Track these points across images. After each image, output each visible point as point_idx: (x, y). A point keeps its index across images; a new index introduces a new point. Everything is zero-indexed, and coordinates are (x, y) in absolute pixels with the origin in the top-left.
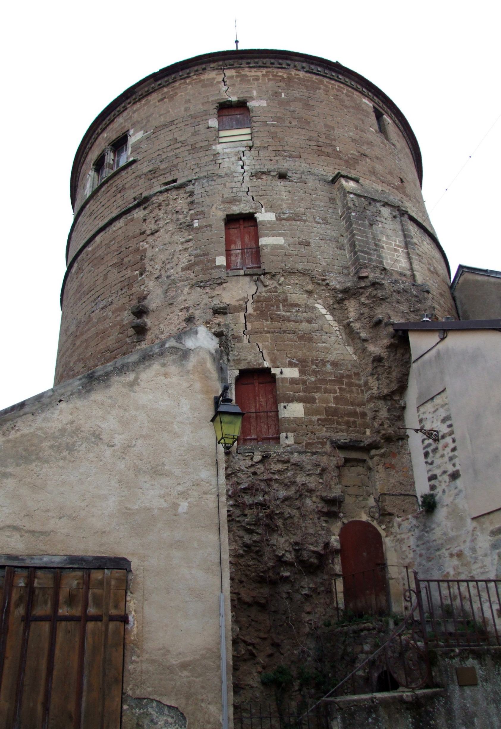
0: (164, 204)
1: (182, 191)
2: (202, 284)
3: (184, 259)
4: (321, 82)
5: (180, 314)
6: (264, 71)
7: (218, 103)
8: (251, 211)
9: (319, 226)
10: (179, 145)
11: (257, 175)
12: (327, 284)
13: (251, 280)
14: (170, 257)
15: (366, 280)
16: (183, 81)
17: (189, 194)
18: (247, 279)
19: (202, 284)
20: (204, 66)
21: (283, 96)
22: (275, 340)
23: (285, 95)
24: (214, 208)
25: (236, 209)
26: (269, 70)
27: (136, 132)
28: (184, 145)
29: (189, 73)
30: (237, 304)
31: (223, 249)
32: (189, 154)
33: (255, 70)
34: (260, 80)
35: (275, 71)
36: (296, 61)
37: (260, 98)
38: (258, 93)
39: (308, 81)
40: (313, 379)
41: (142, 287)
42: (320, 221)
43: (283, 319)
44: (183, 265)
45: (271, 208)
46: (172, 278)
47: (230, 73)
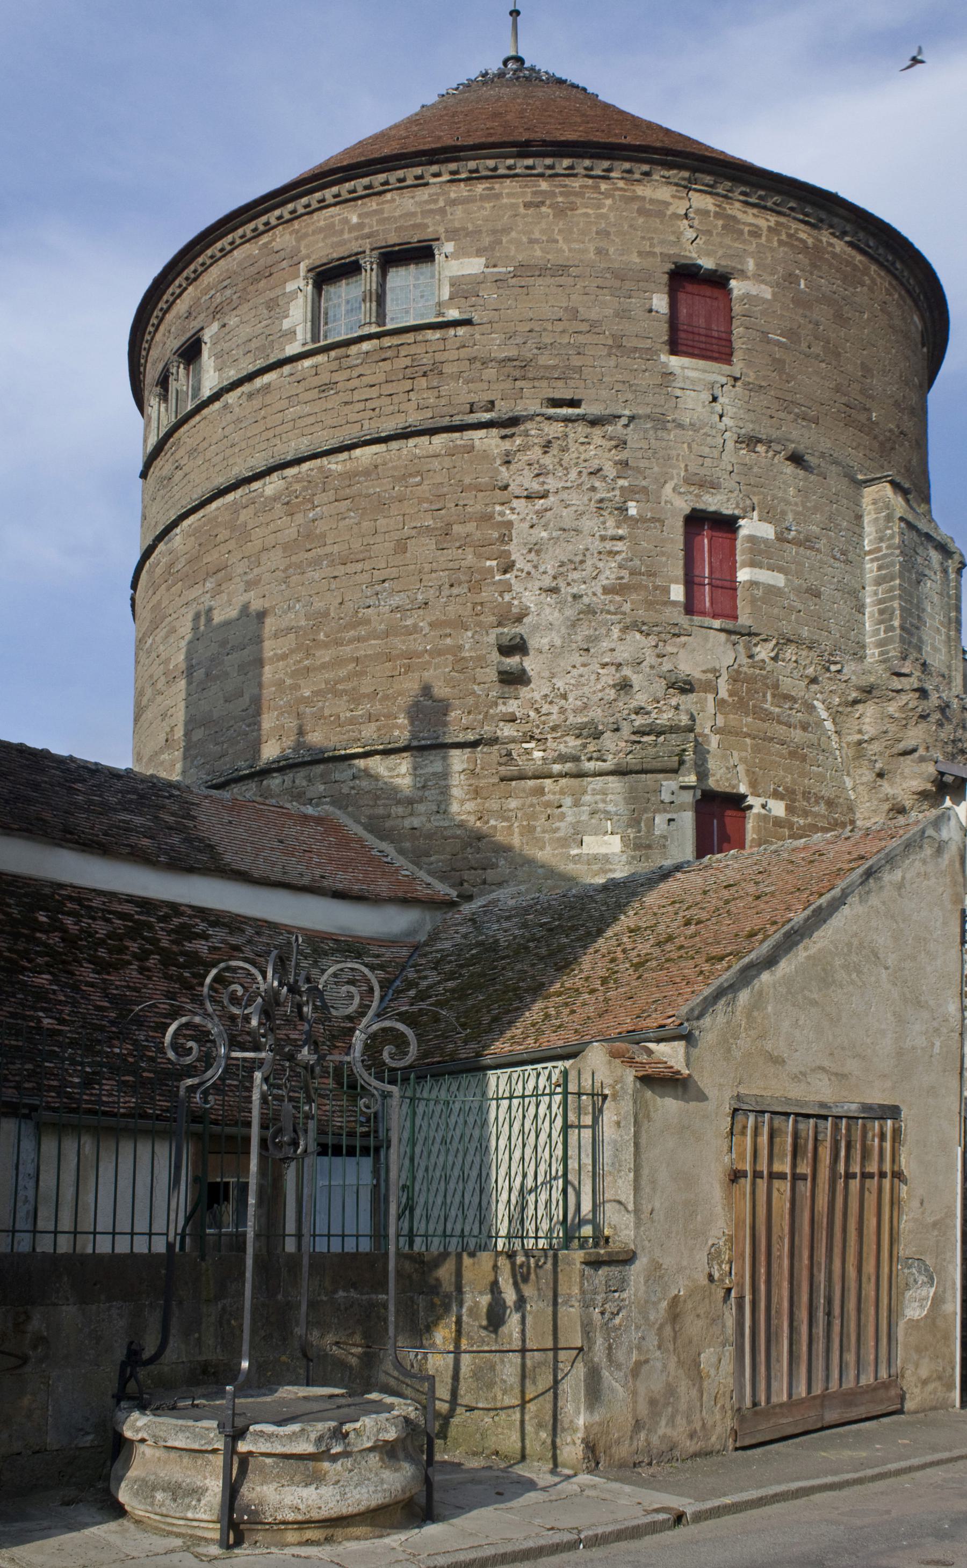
1: (597, 431)
2: (644, 628)
3: (610, 572)
4: (866, 272)
5: (600, 671)
6: (773, 219)
7: (675, 263)
8: (737, 512)
9: (837, 564)
10: (584, 327)
11: (751, 441)
13: (728, 640)
14: (578, 559)
16: (590, 182)
17: (613, 443)
18: (723, 636)
19: (644, 628)
20: (646, 168)
21: (802, 286)
22: (756, 750)
23: (806, 286)
24: (668, 488)
25: (713, 502)
26: (782, 220)
27: (460, 253)
28: (596, 330)
29: (609, 170)
30: (703, 677)
31: (680, 572)
32: (609, 355)
33: (755, 211)
34: (764, 238)
35: (794, 225)
36: (837, 215)
37: (758, 278)
38: (757, 265)
39: (848, 263)
40: (802, 822)
41: (507, 597)
42: (838, 555)
43: (768, 717)
44: (605, 582)
47: (701, 201)
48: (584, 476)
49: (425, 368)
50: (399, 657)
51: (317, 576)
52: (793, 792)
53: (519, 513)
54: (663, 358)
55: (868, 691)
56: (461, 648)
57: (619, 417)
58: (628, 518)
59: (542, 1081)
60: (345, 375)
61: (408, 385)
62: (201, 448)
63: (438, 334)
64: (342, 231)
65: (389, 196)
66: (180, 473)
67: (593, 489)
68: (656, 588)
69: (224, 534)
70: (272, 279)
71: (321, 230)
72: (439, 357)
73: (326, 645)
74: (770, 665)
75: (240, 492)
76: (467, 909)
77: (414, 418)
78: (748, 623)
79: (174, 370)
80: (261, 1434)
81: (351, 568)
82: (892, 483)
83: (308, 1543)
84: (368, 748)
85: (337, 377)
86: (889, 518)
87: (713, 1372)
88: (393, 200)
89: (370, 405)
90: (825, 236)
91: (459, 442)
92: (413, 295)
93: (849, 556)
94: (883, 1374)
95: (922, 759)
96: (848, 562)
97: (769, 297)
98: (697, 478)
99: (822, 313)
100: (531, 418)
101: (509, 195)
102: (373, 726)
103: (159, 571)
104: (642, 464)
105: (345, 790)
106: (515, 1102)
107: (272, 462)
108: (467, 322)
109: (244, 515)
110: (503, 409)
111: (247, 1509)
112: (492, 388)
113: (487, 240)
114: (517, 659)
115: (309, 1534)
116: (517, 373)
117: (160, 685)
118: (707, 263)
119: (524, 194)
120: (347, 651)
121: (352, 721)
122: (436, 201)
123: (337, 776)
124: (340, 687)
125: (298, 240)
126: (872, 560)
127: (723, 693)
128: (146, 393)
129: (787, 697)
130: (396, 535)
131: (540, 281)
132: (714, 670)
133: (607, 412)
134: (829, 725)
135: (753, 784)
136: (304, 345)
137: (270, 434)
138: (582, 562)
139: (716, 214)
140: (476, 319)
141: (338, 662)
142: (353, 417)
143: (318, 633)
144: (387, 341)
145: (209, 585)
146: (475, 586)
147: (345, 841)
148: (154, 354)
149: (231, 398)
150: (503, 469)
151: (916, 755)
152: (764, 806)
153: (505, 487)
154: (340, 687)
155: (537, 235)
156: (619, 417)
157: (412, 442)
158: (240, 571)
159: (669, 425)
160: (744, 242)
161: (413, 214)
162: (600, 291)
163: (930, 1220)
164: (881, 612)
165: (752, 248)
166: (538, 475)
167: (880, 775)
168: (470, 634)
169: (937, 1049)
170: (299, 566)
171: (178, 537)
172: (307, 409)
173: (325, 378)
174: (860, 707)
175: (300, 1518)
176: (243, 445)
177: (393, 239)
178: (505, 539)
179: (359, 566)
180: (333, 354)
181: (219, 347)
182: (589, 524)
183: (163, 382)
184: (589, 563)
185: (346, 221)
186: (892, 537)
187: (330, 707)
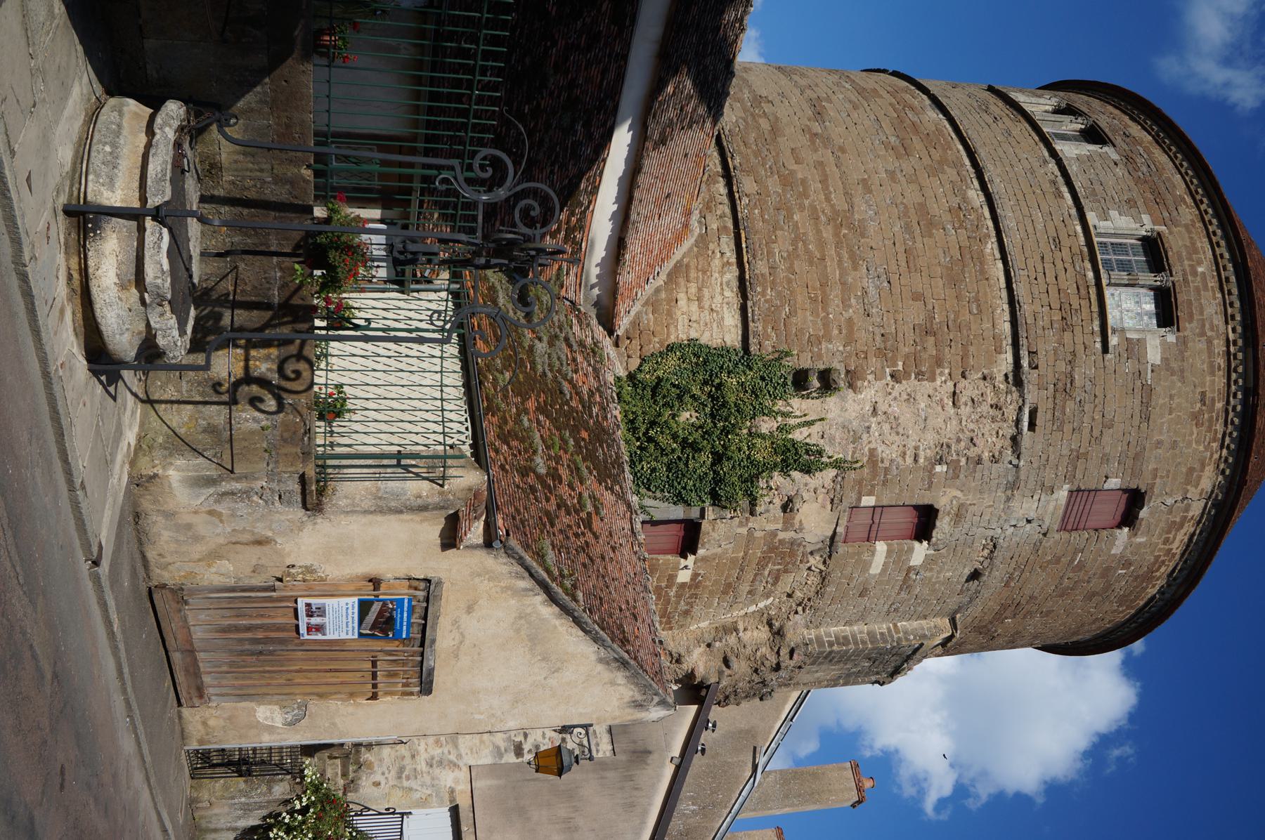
0: (998, 413)
1: (1008, 443)
8: (934, 540)
10: (1096, 433)
12: (796, 613)
14: (901, 431)
15: (788, 656)
17: (997, 454)
18: (830, 533)
24: (959, 494)
25: (943, 526)
26: (1177, 557)
27: (1165, 346)
32: (1071, 450)
41: (870, 377)
44: (880, 450)
45: (929, 561)
46: (865, 436)
47: (1196, 509)
48: (969, 434)
49: (1069, 318)
50: (824, 292)
51: (897, 229)
52: (697, 587)
53: (942, 385)
54: (1067, 487)
55: (779, 633)
56: (830, 341)
57: (1018, 458)
58: (933, 465)
59: (456, 426)
60: (1068, 259)
61: (1056, 305)
62: (1010, 139)
63: (1097, 328)
64: (1190, 259)
65: (1219, 295)
66: (991, 121)
67: (959, 440)
68: (873, 486)
69: (936, 155)
70: (1152, 204)
71: (1193, 244)
72: (1078, 330)
73: (836, 235)
74: (804, 567)
75: (971, 170)
76: (607, 342)
77: (1026, 310)
78: (840, 550)
79: (1080, 120)
80: (161, 238)
81: (902, 258)
82: (952, 636)
83: (70, 277)
84: (747, 266)
85: (1065, 251)
86: (924, 636)
87: (213, 570)
88: (1215, 299)
89: (1040, 276)
90: (1160, 583)
91: (1004, 343)
92: (1130, 308)
93: (893, 611)
94: (211, 691)
95: (721, 673)
96: (888, 613)
97: (1113, 552)
98: (963, 512)
99: (1097, 584)
100: (1022, 396)
101: (1213, 382)
102: (766, 271)
103: (907, 97)
104: (978, 475)
105: (711, 246)
106: (438, 403)
107: (995, 197)
108: (1105, 349)
109: (951, 173)
110: (1029, 376)
111: (97, 226)
112: (1050, 367)
113: (1174, 365)
114: (817, 384)
115: (76, 276)
116: (1060, 385)
117: (808, 92)
118: (1143, 513)
119: (1213, 391)
120: (831, 251)
121: (770, 253)
122: (1212, 329)
123: (724, 239)
124: (800, 244)
125: (1186, 226)
126: (889, 629)
127: (781, 535)
128: (1062, 94)
129: (777, 579)
130: (928, 294)
131: (1137, 401)
132: (801, 529)
133: (1023, 450)
134: (753, 608)
135: (704, 559)
136: (1095, 227)
137: (1020, 197)
138: (898, 433)
139: (1186, 517)
140: (1109, 356)
141: (822, 244)
142: (1030, 262)
143: (849, 229)
144: (1093, 291)
145: (893, 139)
146: (881, 353)
147: (668, 247)
148: (1096, 103)
149: (1052, 166)
150: (980, 375)
151: (724, 669)
152: (686, 567)
153: (964, 376)
154: (800, 244)
155: (1177, 400)
156: (1018, 458)
157: (1006, 307)
158: (904, 166)
159: (1009, 492)
160: (1160, 535)
161: (1202, 313)
162: (1125, 443)
163: (337, 721)
164: (845, 638)
165: (1155, 540)
166: (973, 400)
167: (709, 645)
168: (841, 348)
169: (477, 716)
170: (906, 214)
171: (934, 115)
172: (1040, 227)
173: (1066, 242)
174: (767, 628)
175: (90, 270)
176: (1011, 175)
177: (1181, 297)
178: (920, 375)
179: (904, 264)
180: (1085, 249)
181: (1097, 159)
182: (930, 438)
183: (1069, 110)
184: (896, 438)
185: (1200, 263)
186: (907, 640)
187: (784, 236)
